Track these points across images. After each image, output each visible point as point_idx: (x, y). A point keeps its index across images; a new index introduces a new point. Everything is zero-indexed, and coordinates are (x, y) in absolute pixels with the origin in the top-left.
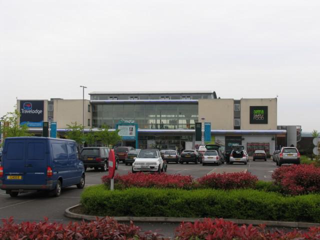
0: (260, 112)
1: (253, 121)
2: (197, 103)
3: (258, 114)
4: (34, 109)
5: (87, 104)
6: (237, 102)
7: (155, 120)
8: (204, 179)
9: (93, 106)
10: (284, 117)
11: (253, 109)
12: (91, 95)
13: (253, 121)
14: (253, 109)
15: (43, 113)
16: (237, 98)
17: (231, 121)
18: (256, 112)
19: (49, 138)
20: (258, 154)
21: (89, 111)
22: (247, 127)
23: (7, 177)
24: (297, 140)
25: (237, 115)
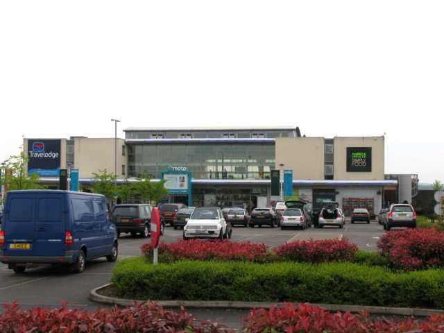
0: (361, 156)
1: (351, 168)
2: (273, 143)
3: (358, 158)
4: (47, 151)
5: (121, 144)
6: (329, 142)
7: (215, 167)
9: (129, 147)
10: (395, 162)
11: (350, 151)
12: (127, 132)
13: (351, 168)
14: (350, 151)
15: (59, 156)
19: (69, 191)
21: (124, 154)
24: (413, 194)
25: (329, 159)
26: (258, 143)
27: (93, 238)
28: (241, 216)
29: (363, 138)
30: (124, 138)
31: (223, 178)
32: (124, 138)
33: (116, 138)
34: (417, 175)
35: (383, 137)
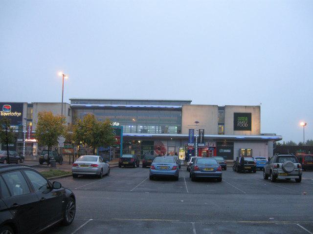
0: (243, 119)
1: (237, 128)
2: (180, 110)
3: (242, 122)
4: (13, 111)
5: (68, 107)
6: (222, 109)
7: (135, 126)
8: (7, 220)
9: (73, 109)
10: (267, 125)
11: (237, 116)
12: (72, 100)
13: (237, 128)
14: (237, 116)
15: (22, 115)
16: (221, 105)
17: (215, 127)
18: (240, 118)
19: (196, 157)
20: (84, 165)
21: (69, 115)
22: (230, 133)
23: (15, 185)
24: (274, 147)
25: (222, 123)
26: (173, 110)
27: (54, 223)
28: (37, 164)
29: (246, 106)
30: (70, 103)
31: (162, 133)
32: (70, 103)
33: (62, 103)
34: (204, 130)
35: (259, 107)
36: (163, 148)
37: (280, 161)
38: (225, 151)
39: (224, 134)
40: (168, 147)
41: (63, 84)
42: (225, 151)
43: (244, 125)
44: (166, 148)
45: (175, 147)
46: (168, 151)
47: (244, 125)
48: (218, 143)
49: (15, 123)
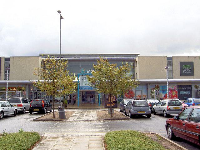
1: (183, 74)
6: (170, 60)
11: (182, 64)
14: (182, 64)
18: (184, 66)
35: (181, 63)
36: (132, 92)
37: (149, 98)
38: (185, 93)
39: (172, 78)
40: (136, 91)
41: (60, 51)
42: (185, 93)
43: (188, 71)
44: (134, 91)
45: (142, 91)
46: (136, 94)
47: (188, 71)
48: (179, 86)
49: (112, 106)
